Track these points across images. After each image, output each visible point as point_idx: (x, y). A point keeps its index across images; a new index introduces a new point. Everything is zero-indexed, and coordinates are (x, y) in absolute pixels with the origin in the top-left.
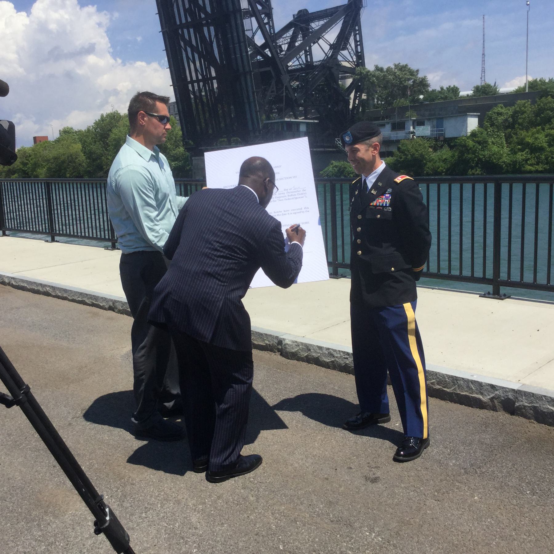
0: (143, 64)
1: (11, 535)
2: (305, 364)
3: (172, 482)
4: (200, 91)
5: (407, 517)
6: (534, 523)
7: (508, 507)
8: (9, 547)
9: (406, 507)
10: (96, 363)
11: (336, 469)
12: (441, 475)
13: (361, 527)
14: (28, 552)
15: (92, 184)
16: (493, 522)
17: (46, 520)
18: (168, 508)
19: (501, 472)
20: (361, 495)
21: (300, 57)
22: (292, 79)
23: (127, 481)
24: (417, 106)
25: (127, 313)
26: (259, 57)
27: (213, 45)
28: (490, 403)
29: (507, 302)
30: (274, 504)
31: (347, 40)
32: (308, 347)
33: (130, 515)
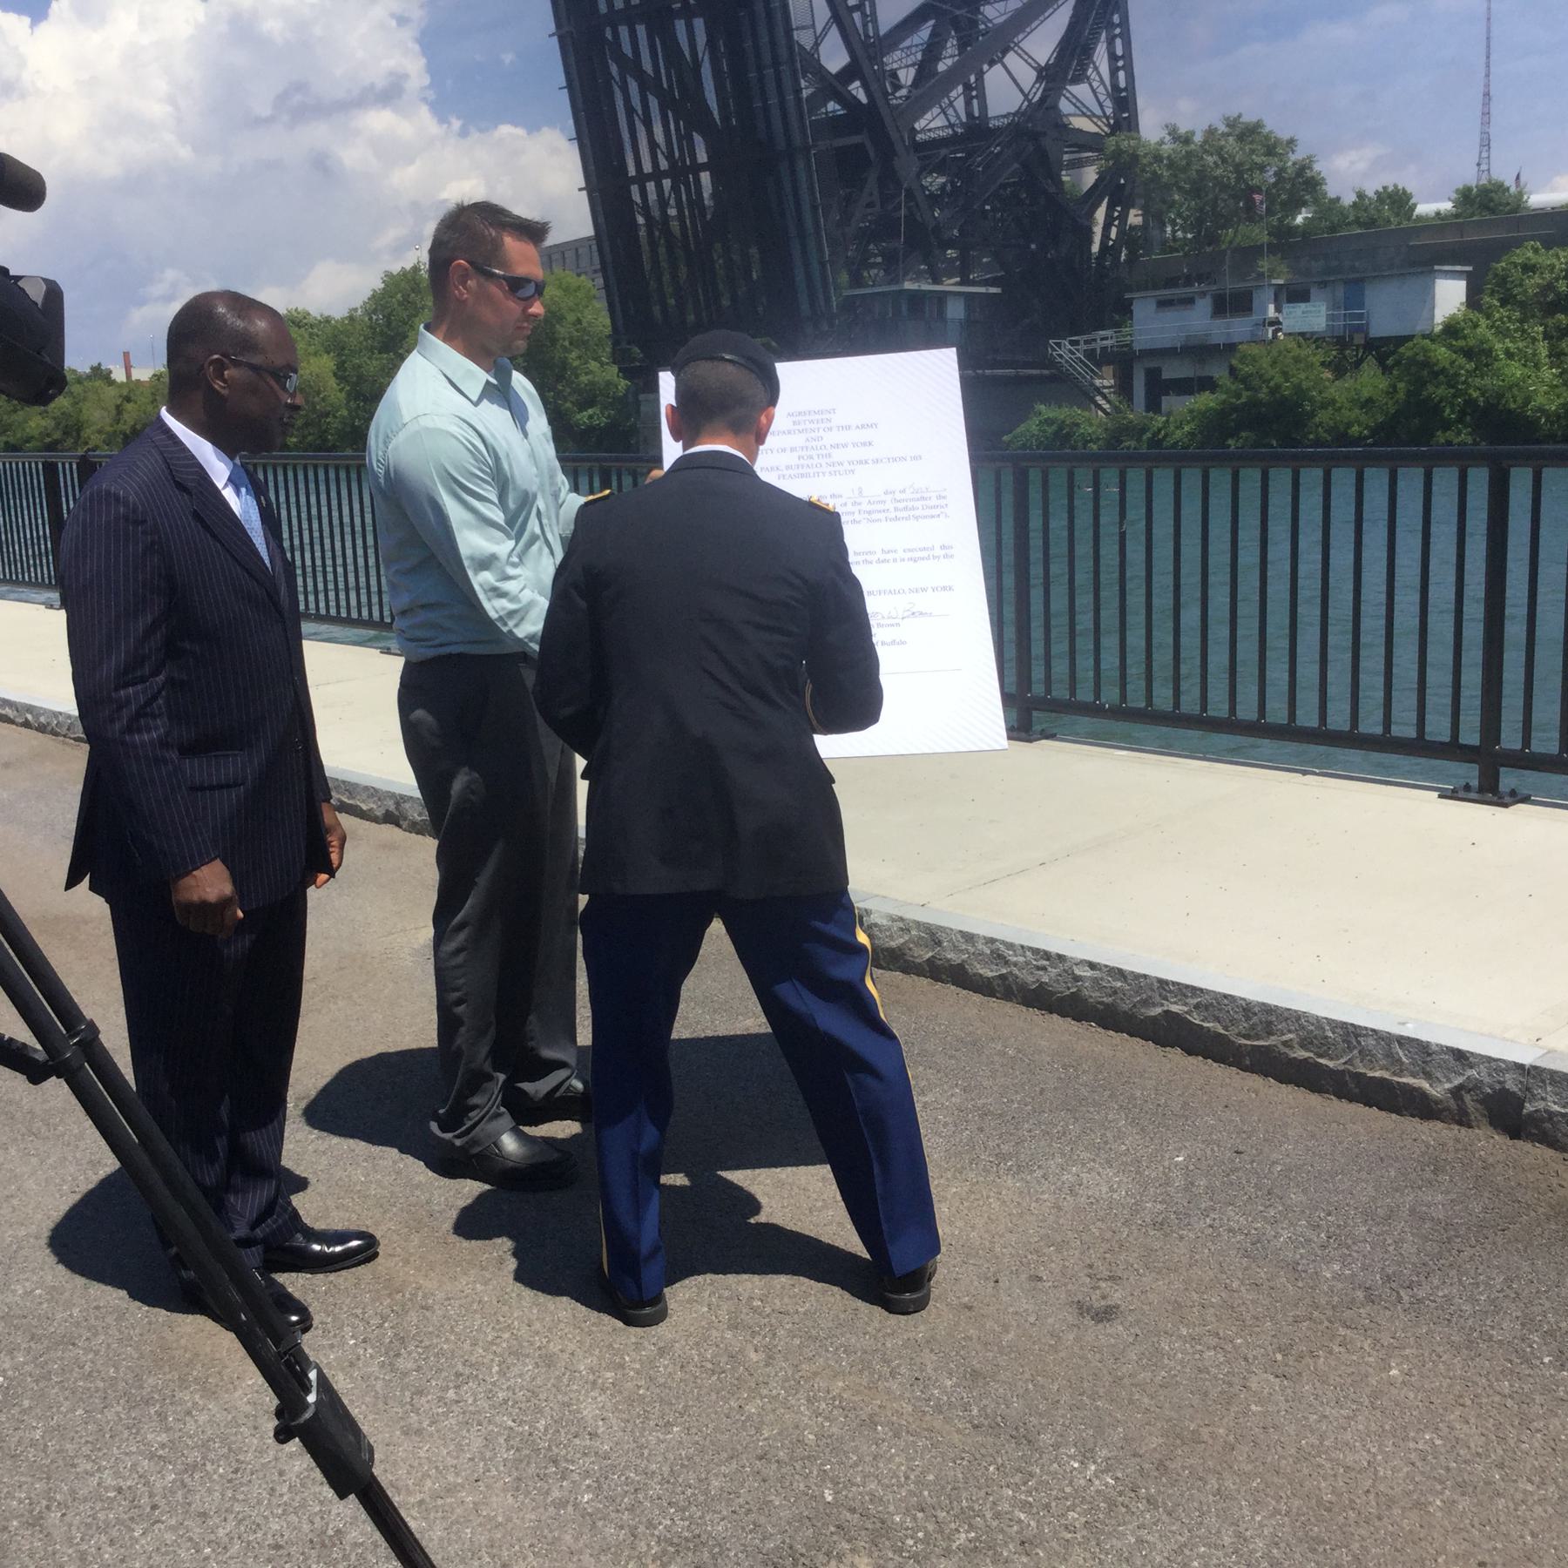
0: (520, 131)
1: (83, 1441)
2: (924, 981)
3: (534, 1303)
4: (663, 203)
5: (1192, 1419)
6: (1557, 1448)
7: (1484, 1400)
8: (78, 1474)
9: (1192, 1393)
10: (341, 969)
11: (997, 1282)
12: (1296, 1305)
13: (1056, 1446)
14: (130, 1488)
15: (316, 467)
16: (1438, 1442)
17: (182, 1402)
18: (521, 1375)
19: (1473, 1300)
20: (1063, 1354)
21: (951, 104)
22: (925, 169)
23: (411, 1300)
24: (1286, 242)
25: (415, 828)
26: (832, 106)
27: (703, 70)
28: (1452, 1104)
29: (1520, 813)
30: (815, 1374)
31: (1087, 52)
32: (933, 935)
33: (413, 1394)
